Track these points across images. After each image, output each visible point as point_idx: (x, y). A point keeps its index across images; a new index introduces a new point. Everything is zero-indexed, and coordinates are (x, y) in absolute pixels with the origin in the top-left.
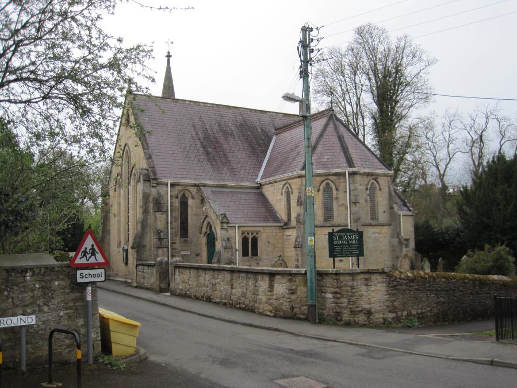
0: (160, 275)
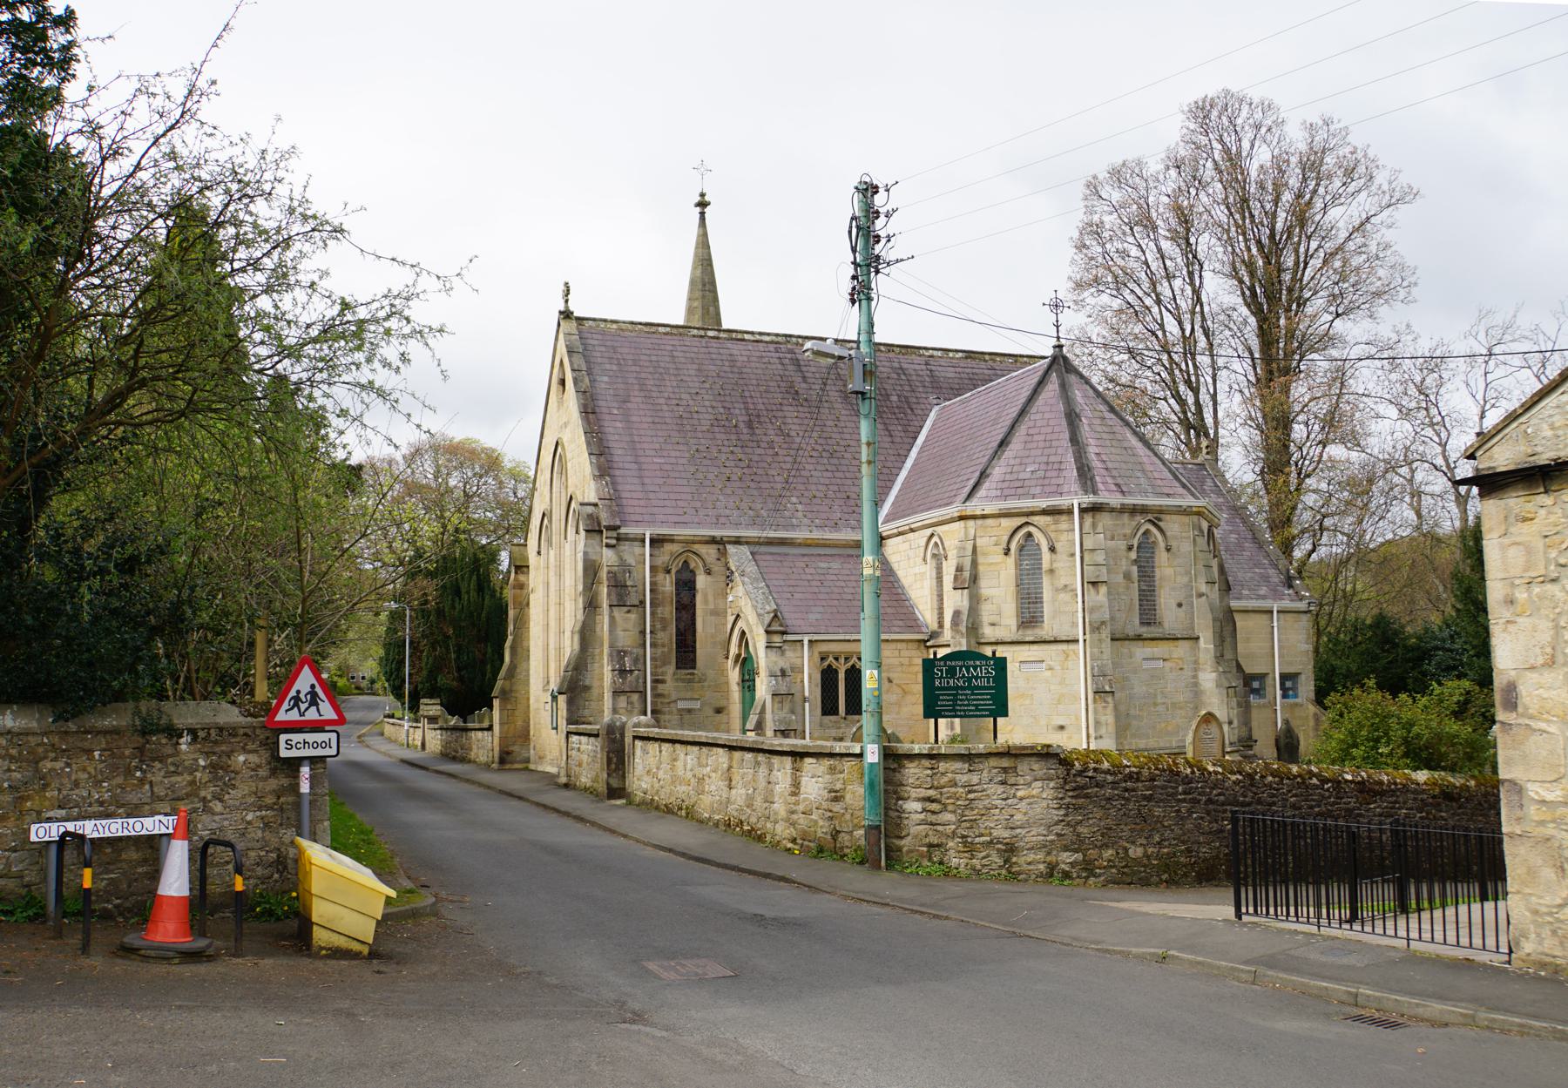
0: (608, 757)
